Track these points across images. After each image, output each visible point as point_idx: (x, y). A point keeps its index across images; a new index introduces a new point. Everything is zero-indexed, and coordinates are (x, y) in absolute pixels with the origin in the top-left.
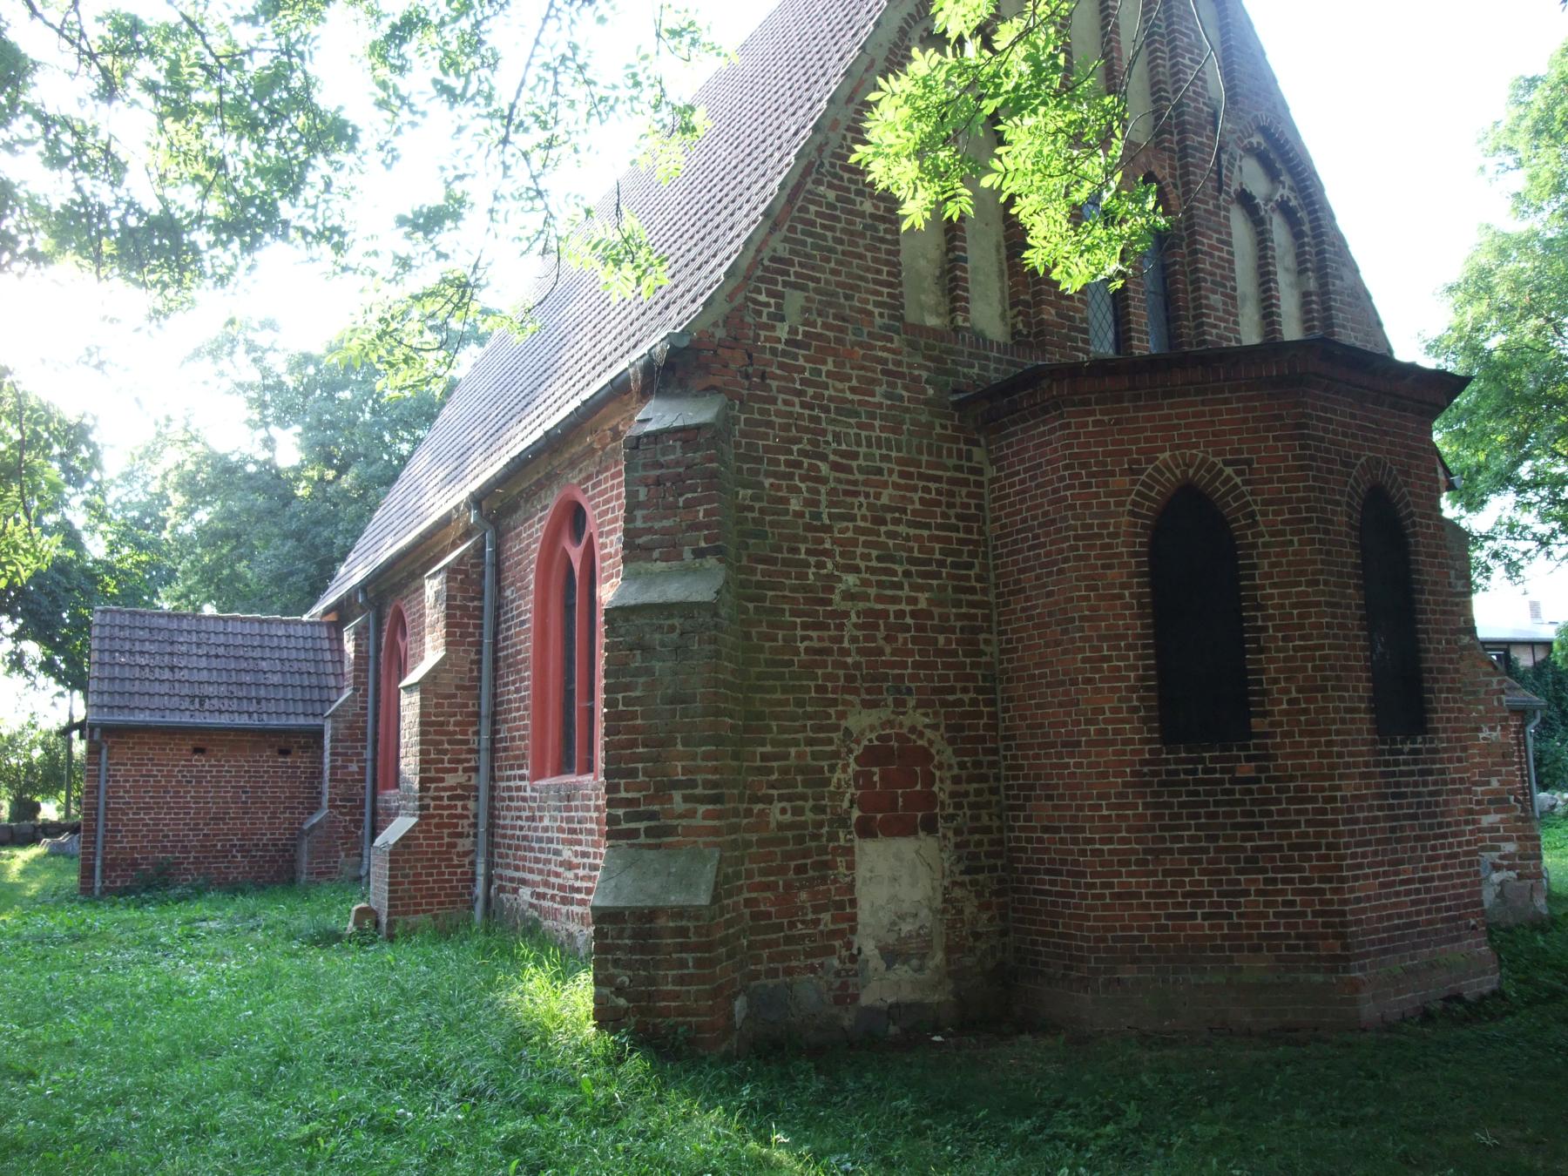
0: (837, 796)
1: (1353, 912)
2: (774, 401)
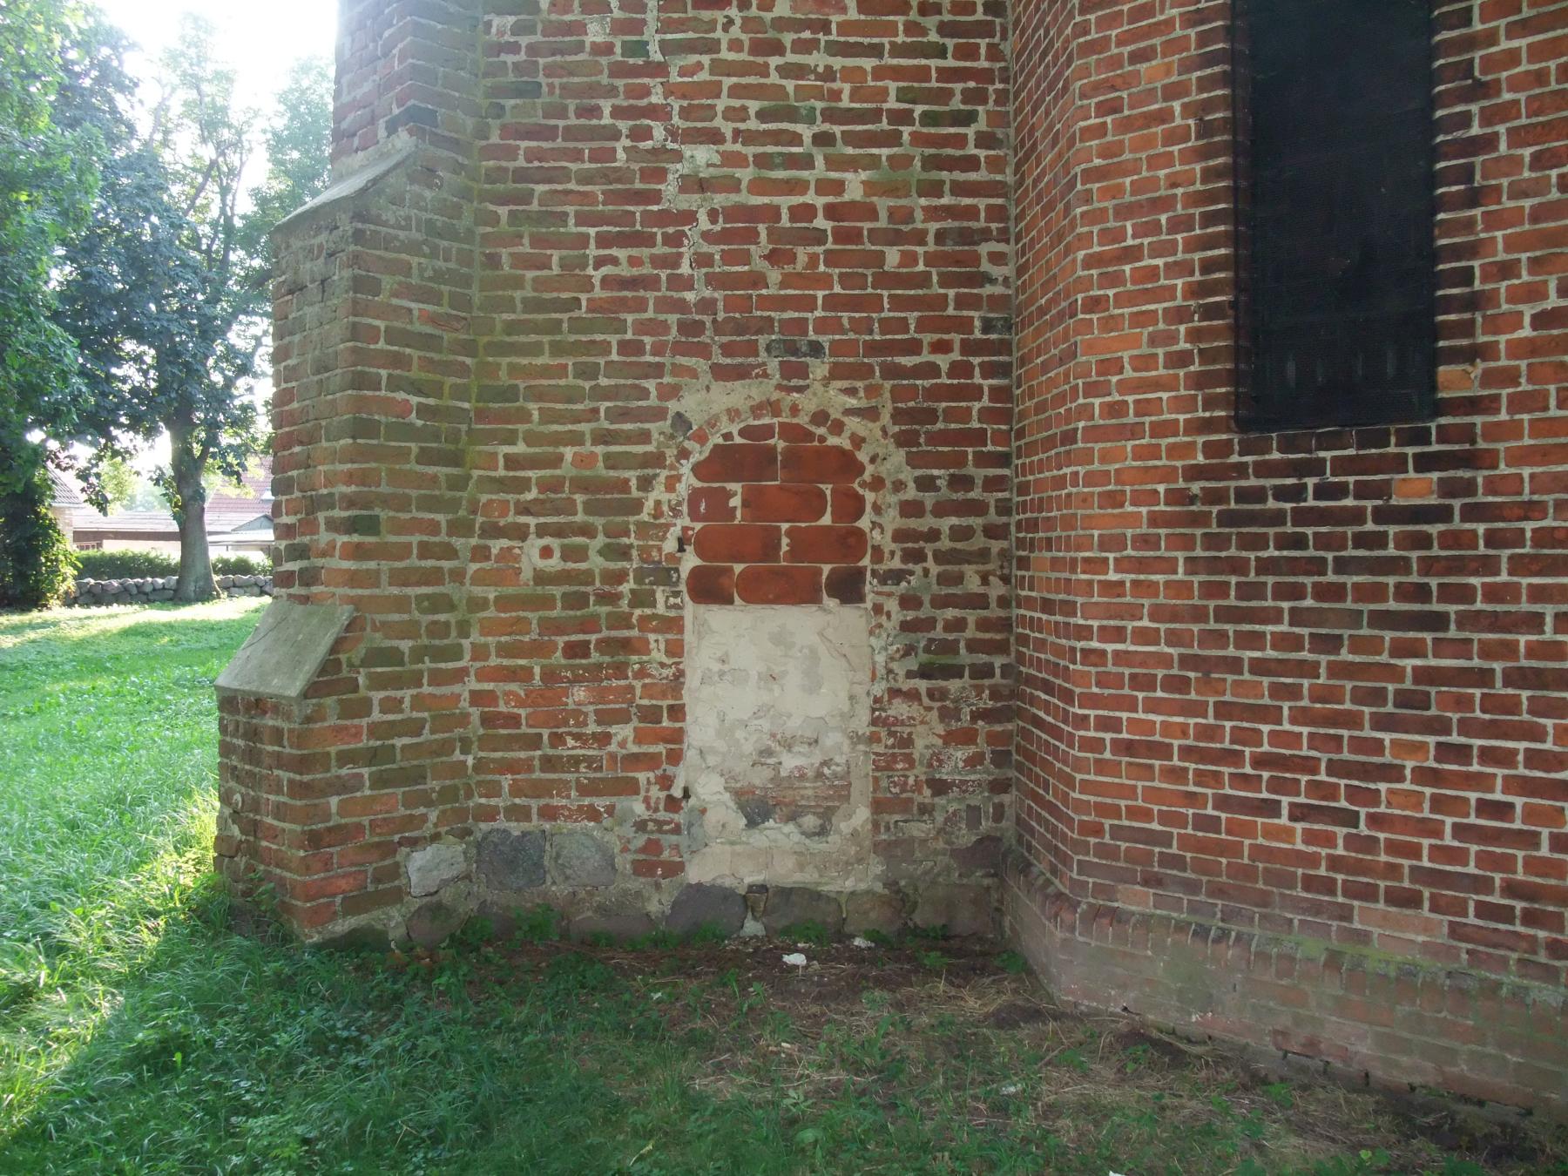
0: (657, 529)
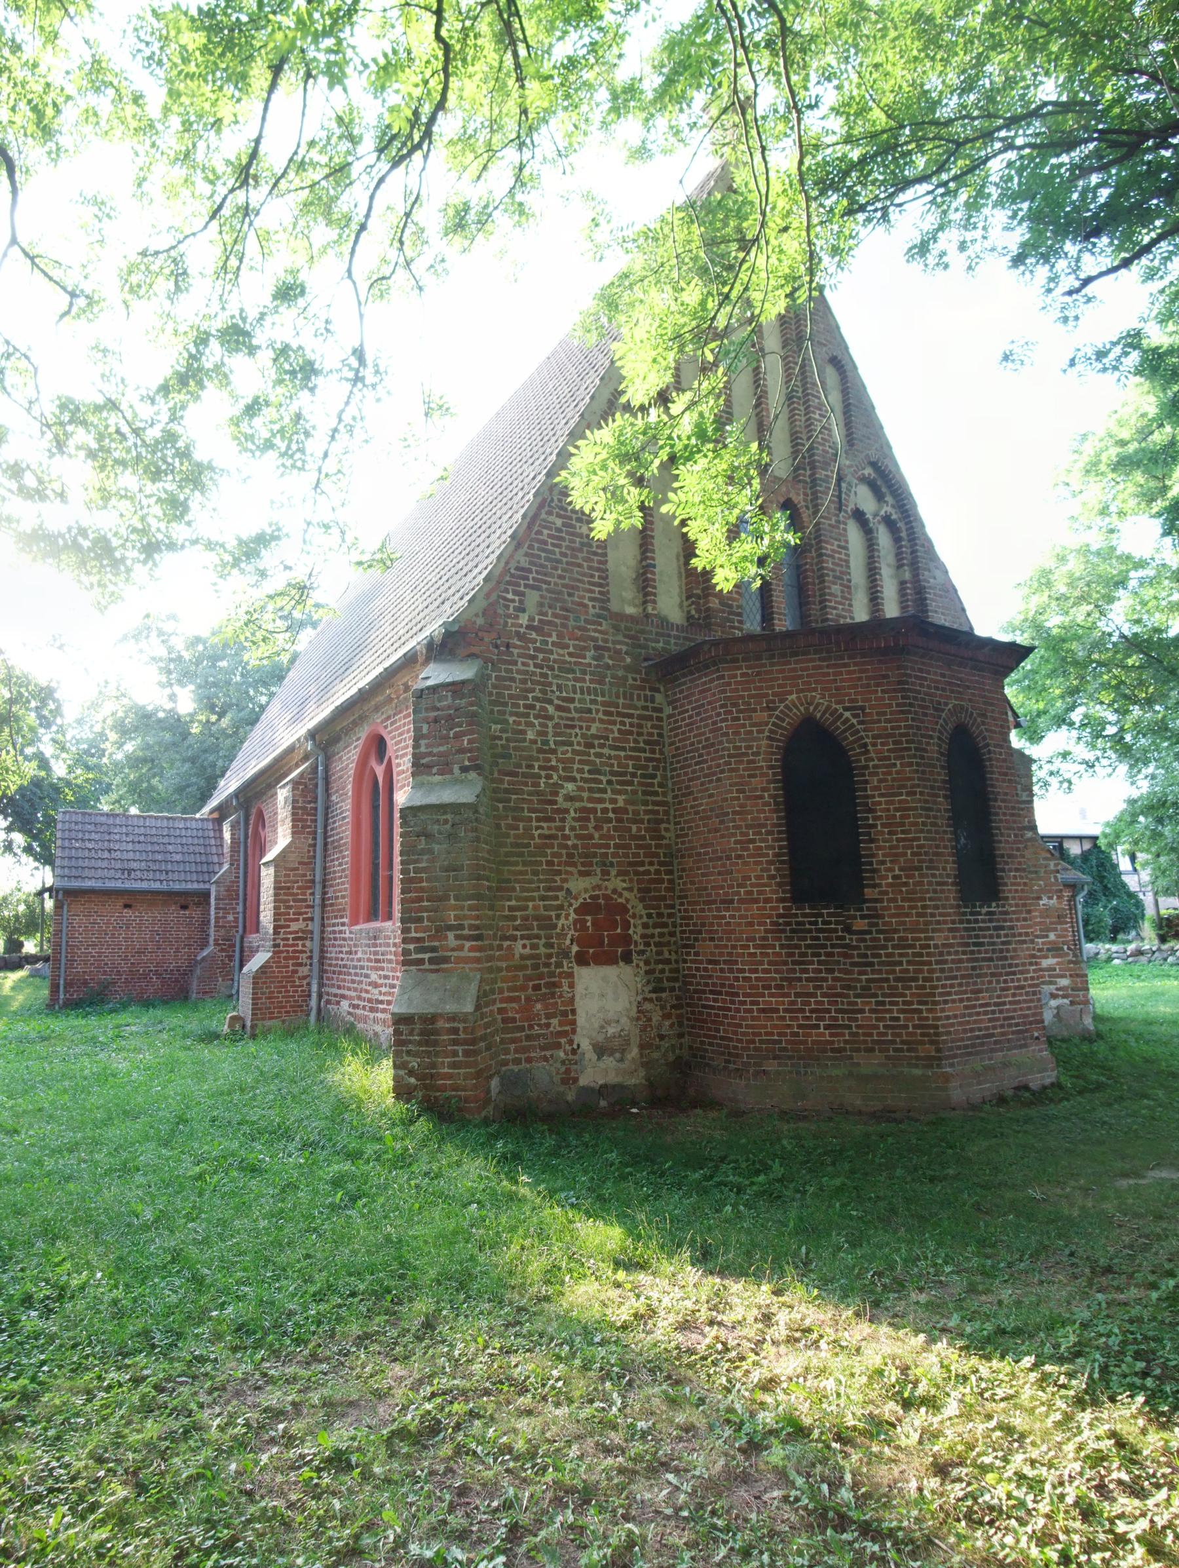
0: (561, 936)
1: (944, 1026)
2: (516, 663)
